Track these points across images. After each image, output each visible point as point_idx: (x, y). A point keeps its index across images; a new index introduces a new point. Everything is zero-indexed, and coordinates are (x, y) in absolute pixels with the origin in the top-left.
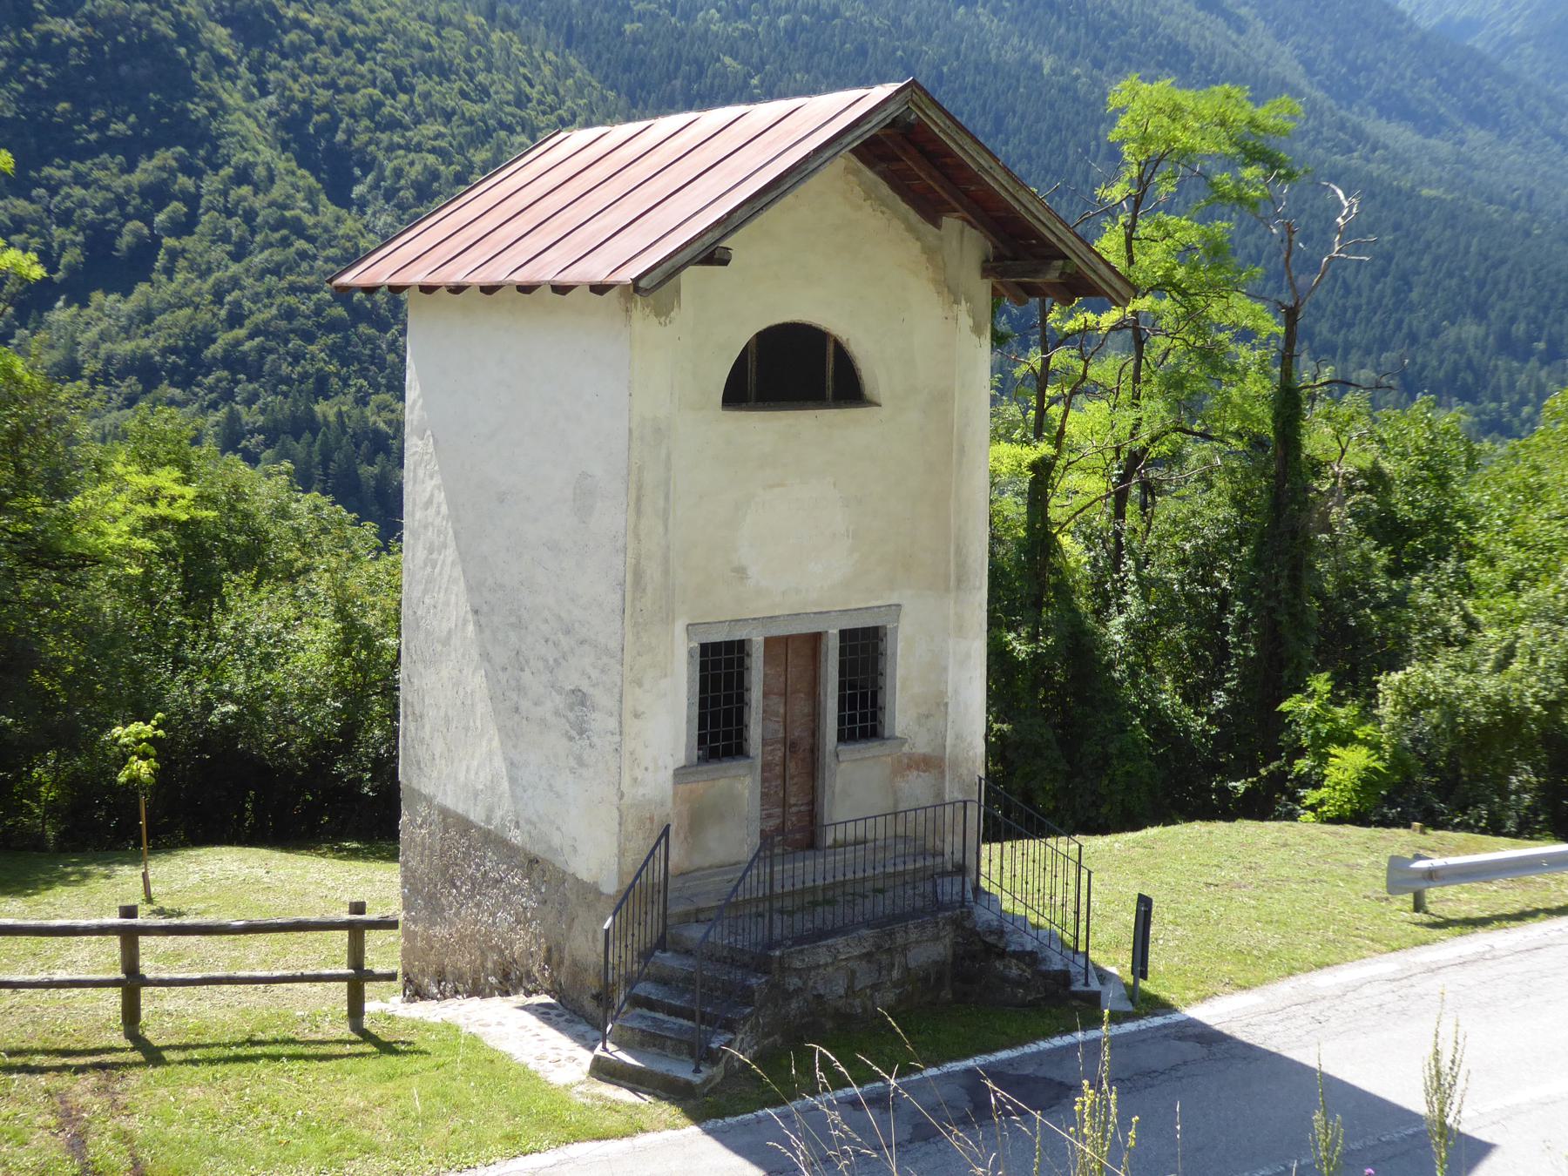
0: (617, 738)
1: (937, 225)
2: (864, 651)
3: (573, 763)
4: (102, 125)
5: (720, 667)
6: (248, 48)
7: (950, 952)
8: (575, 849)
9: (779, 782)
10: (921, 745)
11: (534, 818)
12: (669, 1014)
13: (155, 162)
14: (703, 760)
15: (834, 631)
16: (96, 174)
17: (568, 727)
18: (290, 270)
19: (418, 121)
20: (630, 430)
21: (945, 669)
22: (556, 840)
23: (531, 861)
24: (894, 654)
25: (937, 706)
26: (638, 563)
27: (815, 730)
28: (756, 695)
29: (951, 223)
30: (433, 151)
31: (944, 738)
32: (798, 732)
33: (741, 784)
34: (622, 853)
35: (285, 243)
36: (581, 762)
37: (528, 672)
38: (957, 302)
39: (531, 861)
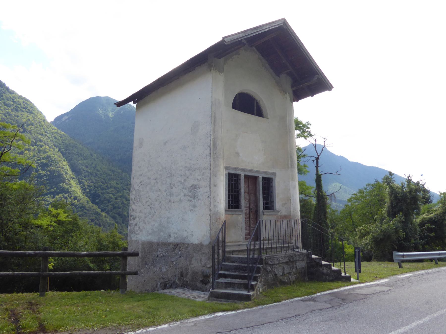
0: (209, 193)
1: (279, 77)
2: (268, 183)
3: (191, 208)
4: (49, 190)
5: (233, 180)
6: (78, 176)
7: (306, 265)
8: (192, 234)
9: (248, 219)
10: (284, 212)
11: (176, 231)
12: (232, 278)
13: (59, 196)
14: (229, 208)
15: (261, 177)
16: (47, 199)
17: (189, 198)
18: (83, 216)
19: (108, 188)
20: (212, 102)
21: (289, 190)
22: (185, 234)
23: (175, 246)
24: (275, 186)
25: (288, 200)
26: (215, 140)
27: (257, 206)
28: (243, 191)
29: (283, 76)
30: (111, 194)
31: (291, 209)
32: (252, 206)
33: (240, 218)
34: (211, 230)
35: (82, 210)
36: (194, 206)
37: (174, 188)
38: (286, 93)
39: (175, 246)
